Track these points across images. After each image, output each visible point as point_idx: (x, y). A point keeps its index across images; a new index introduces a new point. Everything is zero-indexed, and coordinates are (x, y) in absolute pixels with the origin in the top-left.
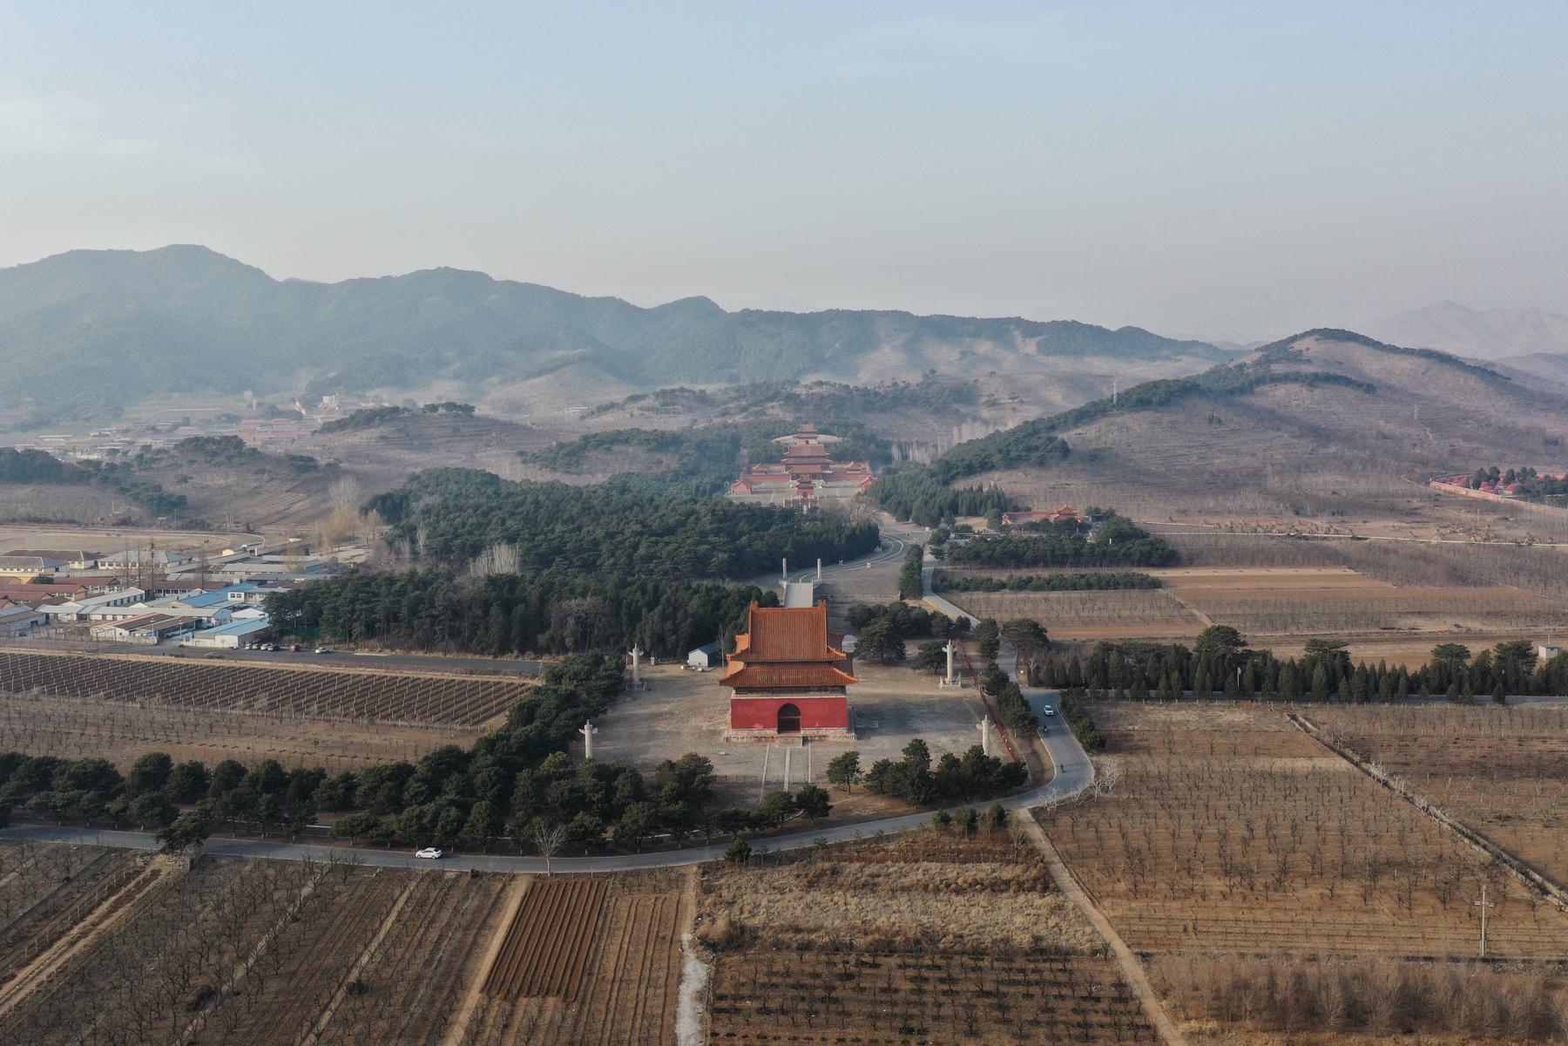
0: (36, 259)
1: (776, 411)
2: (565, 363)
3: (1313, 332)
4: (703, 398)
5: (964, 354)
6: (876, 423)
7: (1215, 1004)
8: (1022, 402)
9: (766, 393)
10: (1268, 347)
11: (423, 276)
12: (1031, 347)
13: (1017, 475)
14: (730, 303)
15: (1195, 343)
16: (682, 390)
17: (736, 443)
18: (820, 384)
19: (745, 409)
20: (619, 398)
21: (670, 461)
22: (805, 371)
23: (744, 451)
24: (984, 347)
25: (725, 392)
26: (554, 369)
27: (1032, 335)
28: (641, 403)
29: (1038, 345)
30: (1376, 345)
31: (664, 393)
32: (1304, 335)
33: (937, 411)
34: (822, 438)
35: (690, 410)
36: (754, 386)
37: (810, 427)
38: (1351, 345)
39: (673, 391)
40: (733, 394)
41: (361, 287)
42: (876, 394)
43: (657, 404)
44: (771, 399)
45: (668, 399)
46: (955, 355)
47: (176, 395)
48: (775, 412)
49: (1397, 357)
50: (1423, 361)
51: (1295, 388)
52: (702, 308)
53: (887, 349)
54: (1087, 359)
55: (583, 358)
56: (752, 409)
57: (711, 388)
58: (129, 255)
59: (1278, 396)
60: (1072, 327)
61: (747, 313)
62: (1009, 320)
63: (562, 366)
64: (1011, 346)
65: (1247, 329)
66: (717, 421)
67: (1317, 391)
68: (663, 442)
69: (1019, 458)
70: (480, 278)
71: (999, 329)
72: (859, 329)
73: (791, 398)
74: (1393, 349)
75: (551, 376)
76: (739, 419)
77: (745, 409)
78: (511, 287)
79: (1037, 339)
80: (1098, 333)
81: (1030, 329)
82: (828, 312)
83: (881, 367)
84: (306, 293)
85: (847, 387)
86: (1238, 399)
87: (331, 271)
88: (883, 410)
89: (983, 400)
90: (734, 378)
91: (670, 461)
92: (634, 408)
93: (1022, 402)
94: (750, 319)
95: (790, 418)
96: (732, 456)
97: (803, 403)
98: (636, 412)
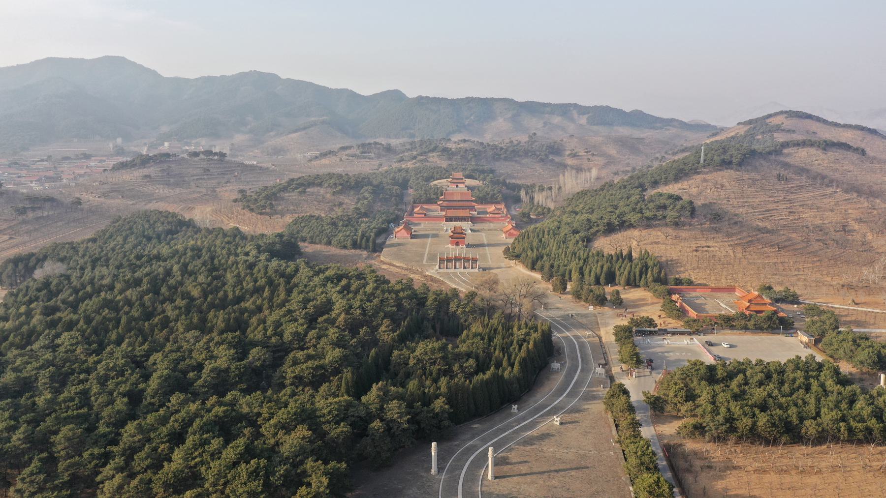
0: (28, 62)
1: (436, 160)
2: (314, 124)
3: (782, 112)
4: (389, 149)
5: (545, 124)
6: (503, 168)
7: (545, 300)
8: (593, 155)
9: (428, 147)
10: (750, 122)
11: (243, 75)
12: (583, 120)
13: (657, 234)
14: (411, 93)
15: (673, 120)
16: (376, 143)
17: (404, 185)
18: (465, 141)
19: (415, 158)
20: (336, 146)
21: (350, 202)
22: (454, 132)
23: (411, 191)
24: (557, 120)
25: (403, 145)
26: (304, 129)
27: (584, 114)
28: (348, 152)
29: (588, 119)
30: (825, 122)
31: (363, 145)
32: (776, 114)
33: (542, 160)
34: (470, 182)
35: (379, 156)
36: (422, 142)
37: (459, 175)
38: (808, 121)
39: (370, 144)
40: (408, 147)
41: (208, 80)
42: (502, 149)
43: (358, 152)
44: (433, 150)
45: (366, 149)
46: (540, 125)
47: (76, 140)
48: (436, 159)
49: (841, 129)
50: (859, 132)
51: (813, 151)
52: (395, 96)
53: (501, 120)
54: (616, 128)
55: (323, 122)
56: (420, 158)
57: (394, 142)
58: (82, 60)
59: (801, 156)
60: (607, 109)
61: (420, 98)
62: (570, 105)
63: (309, 127)
64: (572, 120)
65: (728, 112)
66: (395, 165)
67: (830, 153)
68: (347, 185)
69: (655, 217)
70: (274, 77)
71: (565, 109)
72: (485, 107)
73: (446, 150)
74: (836, 125)
75: (303, 132)
76: (410, 165)
77: (415, 158)
78: (289, 81)
79: (586, 116)
80: (620, 113)
81: (582, 110)
82: (467, 98)
83: (497, 132)
84: (178, 83)
85: (482, 144)
86: (773, 157)
87: (192, 74)
88: (506, 159)
89: (568, 153)
90: (412, 136)
91: (350, 202)
92: (343, 155)
93: (593, 155)
94: (421, 101)
95: (444, 164)
96: (400, 197)
97: (453, 154)
98: (344, 158)
